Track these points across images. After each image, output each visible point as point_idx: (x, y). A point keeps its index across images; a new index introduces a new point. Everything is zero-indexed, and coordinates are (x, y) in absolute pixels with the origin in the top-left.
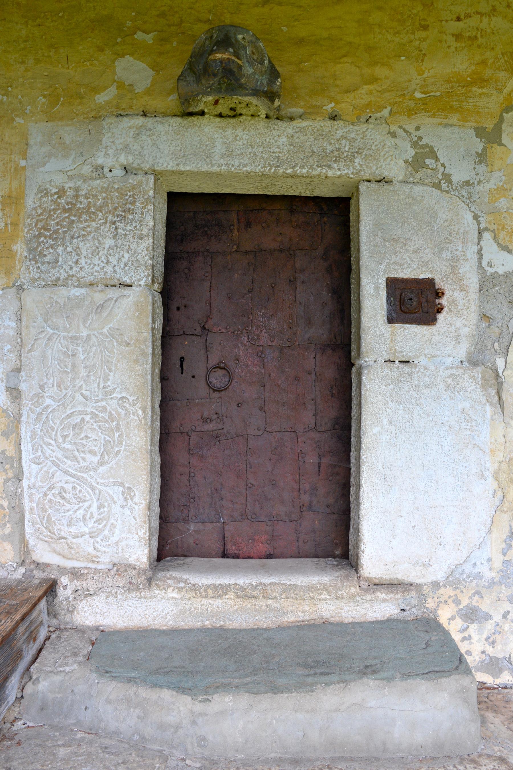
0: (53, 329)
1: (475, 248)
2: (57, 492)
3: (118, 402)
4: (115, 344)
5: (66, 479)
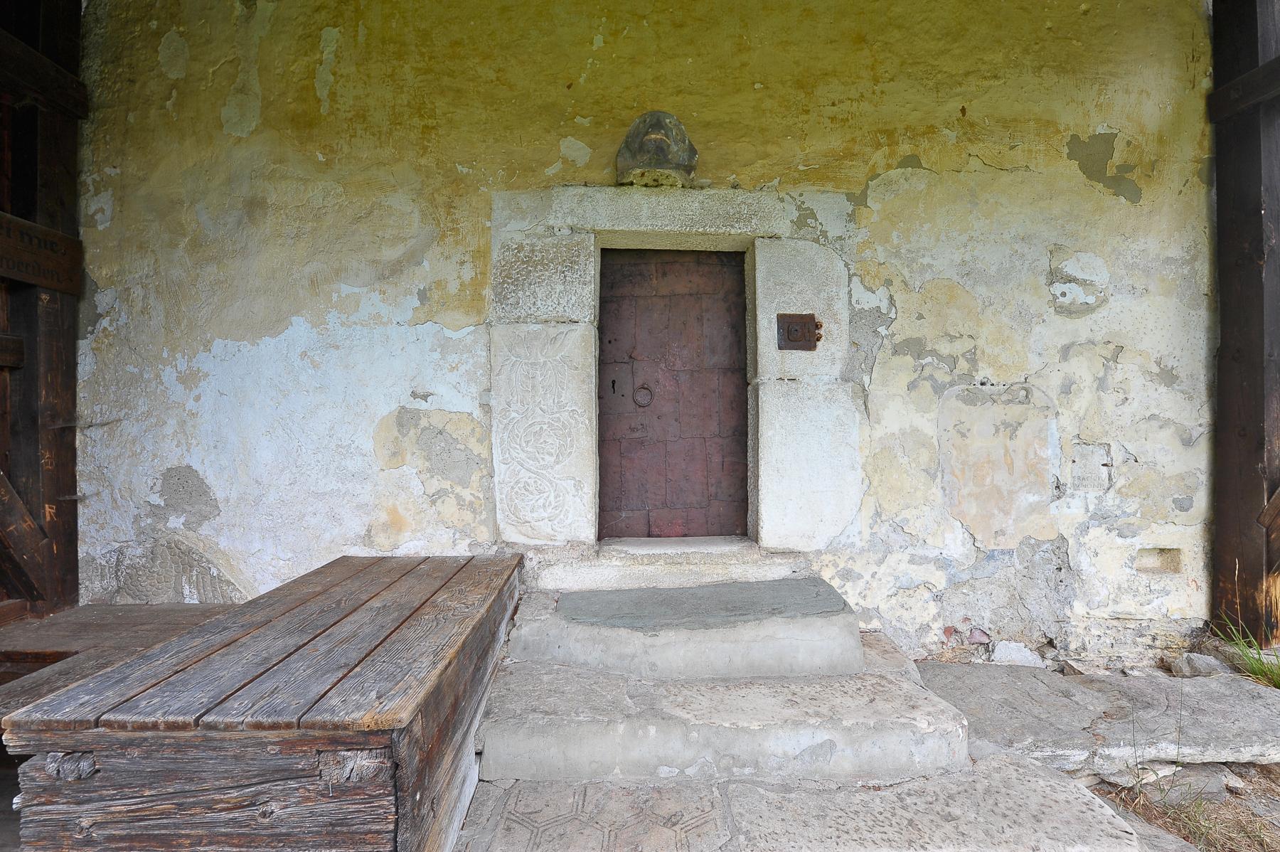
1: (847, 289)
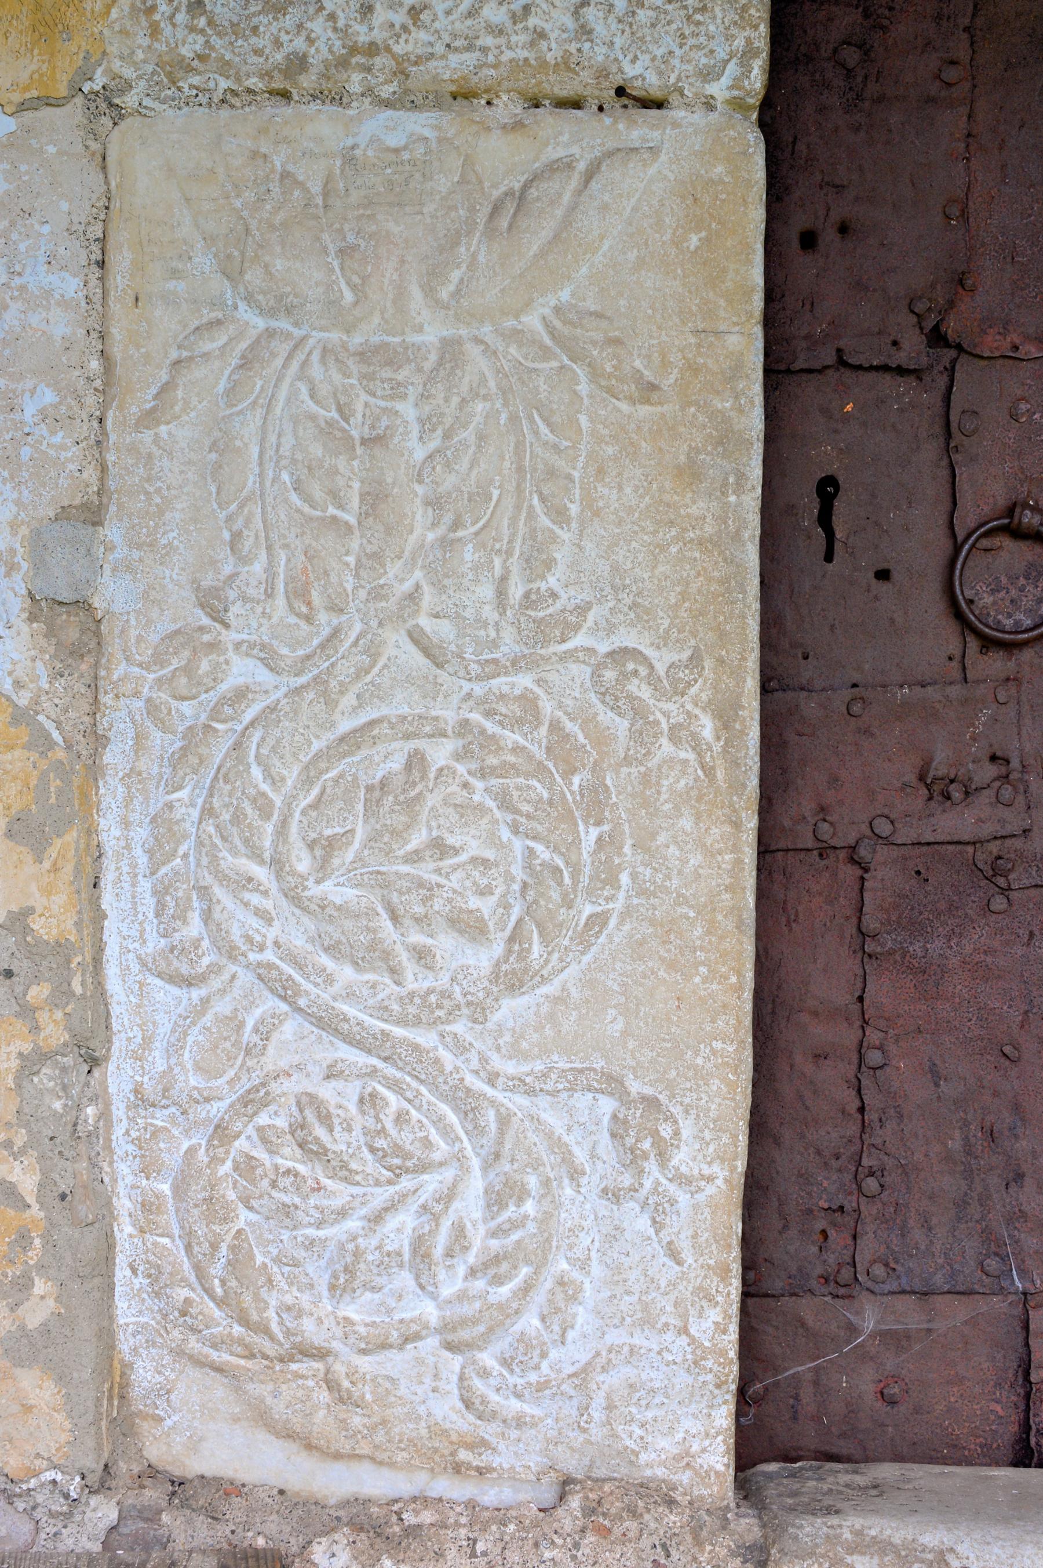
0: (271, 313)
2: (281, 1123)
3: (596, 673)
4: (583, 388)
5: (330, 1056)
